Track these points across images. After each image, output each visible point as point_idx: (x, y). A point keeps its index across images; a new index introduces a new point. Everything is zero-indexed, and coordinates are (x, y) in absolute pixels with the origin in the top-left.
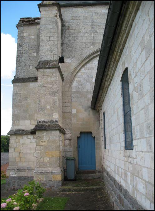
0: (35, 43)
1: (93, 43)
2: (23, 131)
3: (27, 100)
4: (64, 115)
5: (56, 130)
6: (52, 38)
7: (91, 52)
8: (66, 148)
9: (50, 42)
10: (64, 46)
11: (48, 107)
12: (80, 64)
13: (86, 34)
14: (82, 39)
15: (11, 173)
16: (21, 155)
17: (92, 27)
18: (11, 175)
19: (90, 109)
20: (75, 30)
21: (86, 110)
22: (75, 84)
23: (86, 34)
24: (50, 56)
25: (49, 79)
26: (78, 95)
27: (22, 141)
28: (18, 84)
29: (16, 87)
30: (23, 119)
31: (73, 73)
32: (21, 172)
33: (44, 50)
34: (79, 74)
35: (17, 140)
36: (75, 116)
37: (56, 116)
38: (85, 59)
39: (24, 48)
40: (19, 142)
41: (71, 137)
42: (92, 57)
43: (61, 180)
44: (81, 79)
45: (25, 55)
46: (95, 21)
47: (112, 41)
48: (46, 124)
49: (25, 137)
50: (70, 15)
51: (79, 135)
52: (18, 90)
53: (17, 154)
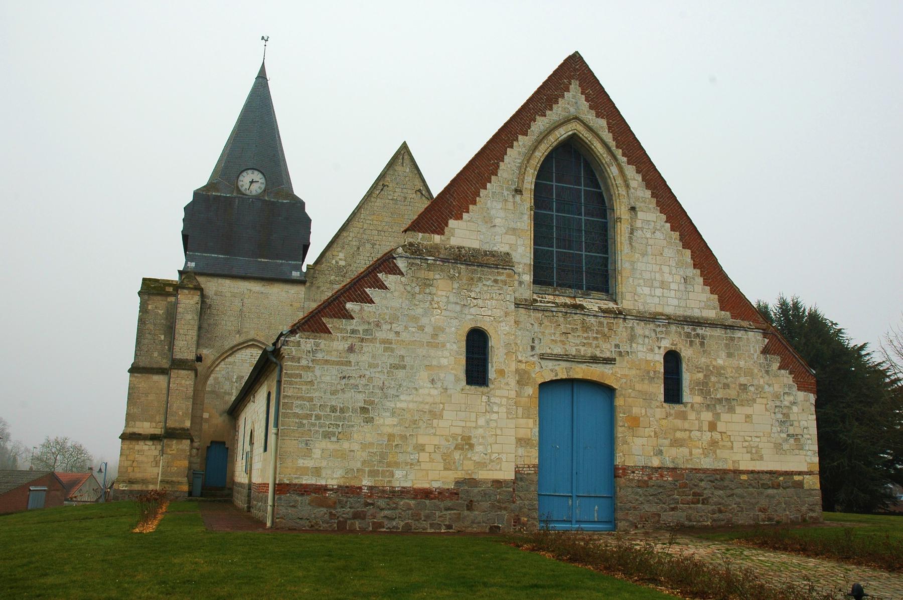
0: (162, 321)
1: (239, 332)
2: (140, 434)
3: (147, 396)
4: (196, 418)
5: (187, 439)
6: (190, 332)
7: (235, 343)
8: (192, 459)
9: (187, 336)
10: (201, 331)
11: (180, 413)
12: (219, 357)
13: (232, 319)
14: (226, 325)
15: (121, 485)
16: (135, 464)
17: (241, 310)
18: (121, 488)
19: (226, 414)
20: (218, 310)
21: (221, 415)
22: (211, 381)
23: (232, 319)
24: (186, 354)
25: (183, 382)
26: (213, 396)
27: (137, 447)
28: (136, 375)
29: (134, 378)
30: (140, 420)
31: (209, 368)
32: (133, 485)
33: (180, 345)
34: (217, 369)
35: (131, 446)
36: (207, 420)
37: (188, 424)
38: (226, 352)
39: (147, 326)
40: (133, 449)
41: (199, 445)
42: (236, 349)
43: (187, 490)
44: (219, 375)
45: (149, 337)
46: (245, 300)
47: (235, 407)
48: (177, 432)
49: (141, 443)
50: (214, 289)
51: (209, 445)
52: (135, 383)
53: (130, 463)
